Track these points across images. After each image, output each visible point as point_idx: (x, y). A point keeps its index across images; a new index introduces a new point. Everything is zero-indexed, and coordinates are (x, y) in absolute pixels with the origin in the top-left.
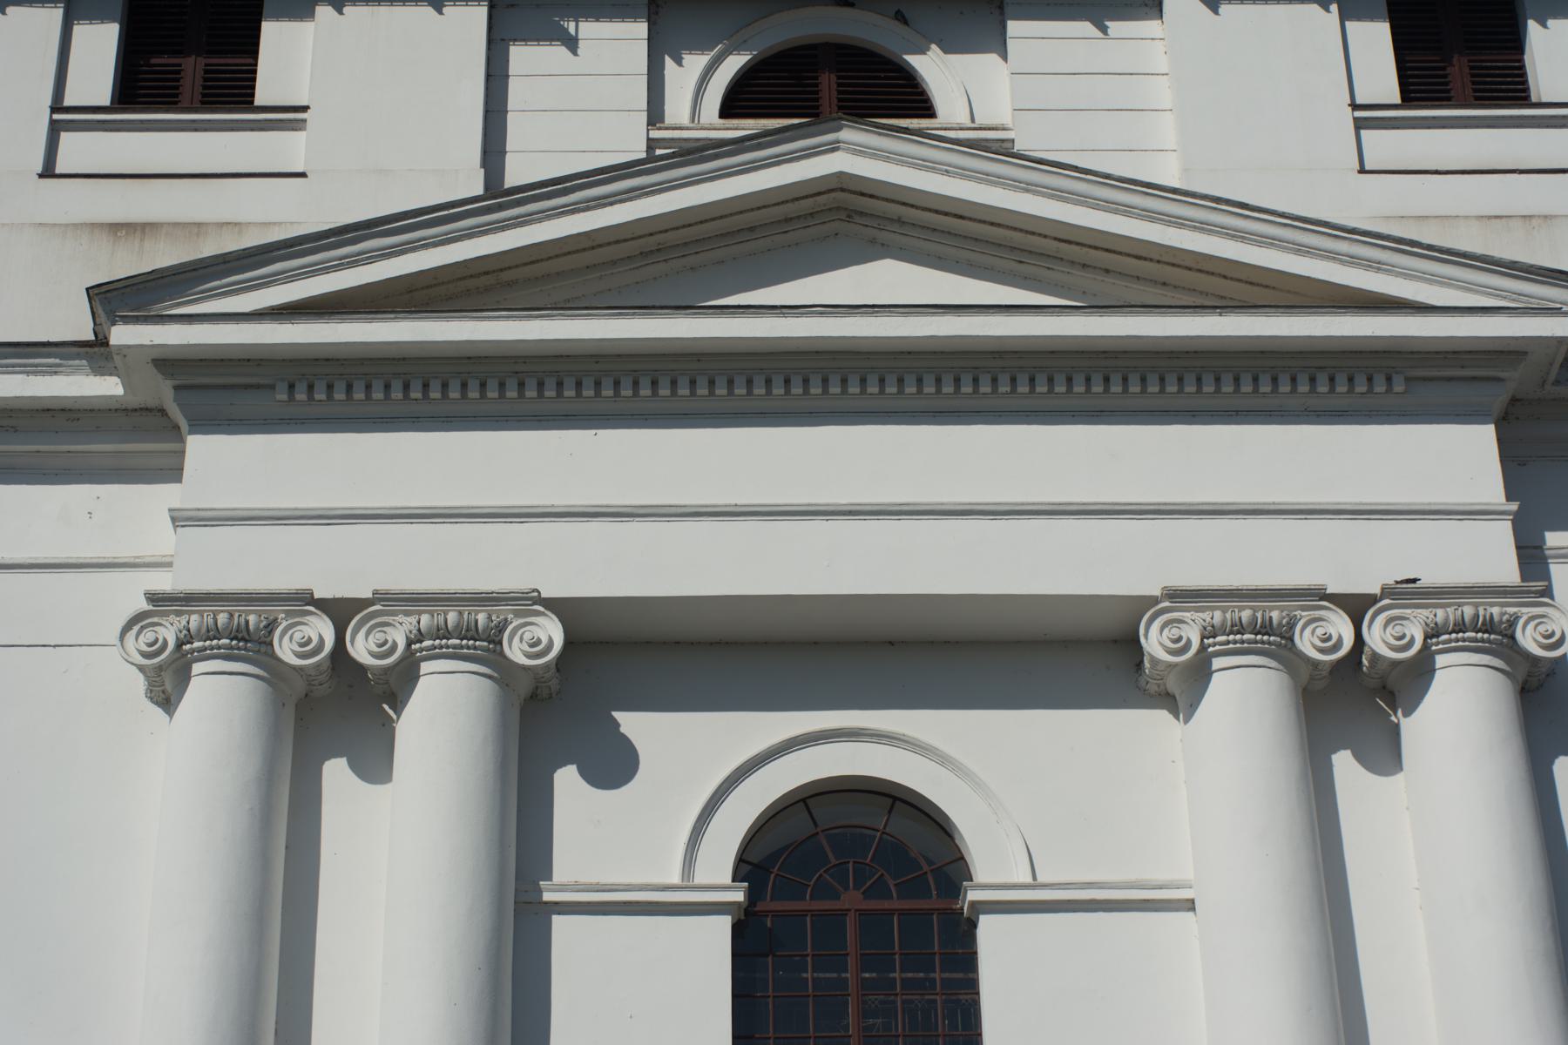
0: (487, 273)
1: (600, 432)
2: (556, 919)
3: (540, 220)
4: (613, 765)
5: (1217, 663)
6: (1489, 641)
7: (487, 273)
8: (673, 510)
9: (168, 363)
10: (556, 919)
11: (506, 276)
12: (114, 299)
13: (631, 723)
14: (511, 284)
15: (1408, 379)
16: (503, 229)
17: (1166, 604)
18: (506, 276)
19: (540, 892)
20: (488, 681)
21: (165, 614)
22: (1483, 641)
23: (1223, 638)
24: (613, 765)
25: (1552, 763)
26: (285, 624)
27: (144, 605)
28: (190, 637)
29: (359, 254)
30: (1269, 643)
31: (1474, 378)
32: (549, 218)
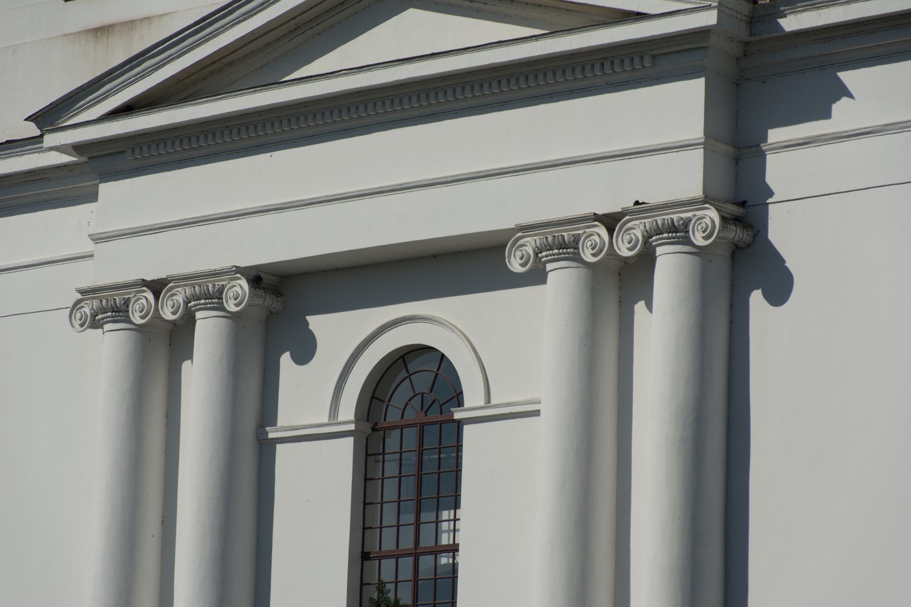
0: (214, 63)
1: (273, 153)
2: (278, 446)
3: (223, 32)
4: (305, 350)
5: (549, 267)
6: (678, 238)
7: (214, 63)
8: (296, 204)
9: (78, 148)
10: (278, 446)
11: (225, 61)
12: (49, 117)
13: (315, 322)
14: (230, 64)
15: (653, 56)
16: (207, 41)
17: (520, 234)
18: (225, 61)
19: (267, 433)
20: (225, 319)
21: (87, 299)
22: (673, 238)
23: (556, 251)
24: (305, 350)
25: (749, 295)
26: (133, 300)
27: (79, 296)
28: (105, 307)
29: (143, 71)
30: (568, 253)
31: (690, 49)
32: (227, 29)
